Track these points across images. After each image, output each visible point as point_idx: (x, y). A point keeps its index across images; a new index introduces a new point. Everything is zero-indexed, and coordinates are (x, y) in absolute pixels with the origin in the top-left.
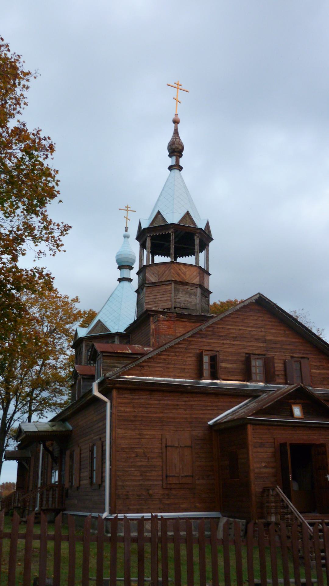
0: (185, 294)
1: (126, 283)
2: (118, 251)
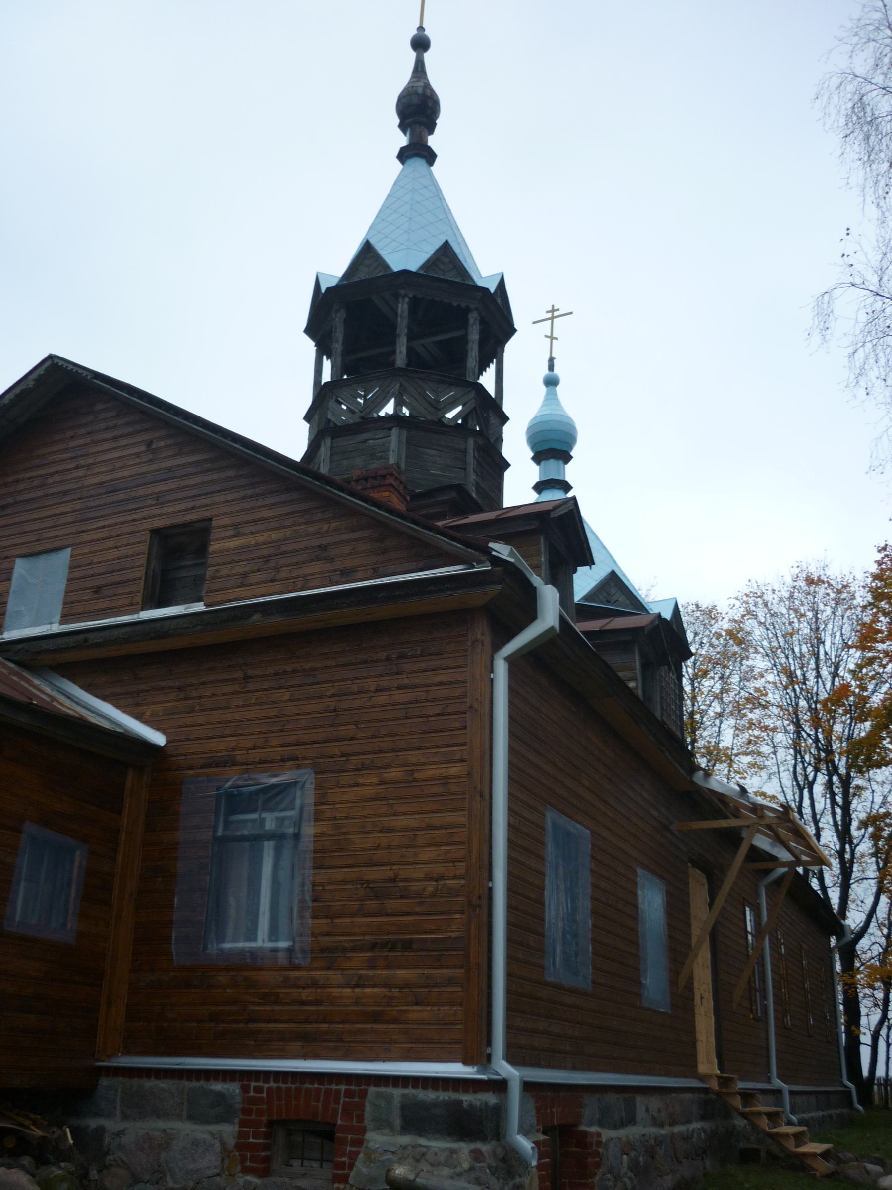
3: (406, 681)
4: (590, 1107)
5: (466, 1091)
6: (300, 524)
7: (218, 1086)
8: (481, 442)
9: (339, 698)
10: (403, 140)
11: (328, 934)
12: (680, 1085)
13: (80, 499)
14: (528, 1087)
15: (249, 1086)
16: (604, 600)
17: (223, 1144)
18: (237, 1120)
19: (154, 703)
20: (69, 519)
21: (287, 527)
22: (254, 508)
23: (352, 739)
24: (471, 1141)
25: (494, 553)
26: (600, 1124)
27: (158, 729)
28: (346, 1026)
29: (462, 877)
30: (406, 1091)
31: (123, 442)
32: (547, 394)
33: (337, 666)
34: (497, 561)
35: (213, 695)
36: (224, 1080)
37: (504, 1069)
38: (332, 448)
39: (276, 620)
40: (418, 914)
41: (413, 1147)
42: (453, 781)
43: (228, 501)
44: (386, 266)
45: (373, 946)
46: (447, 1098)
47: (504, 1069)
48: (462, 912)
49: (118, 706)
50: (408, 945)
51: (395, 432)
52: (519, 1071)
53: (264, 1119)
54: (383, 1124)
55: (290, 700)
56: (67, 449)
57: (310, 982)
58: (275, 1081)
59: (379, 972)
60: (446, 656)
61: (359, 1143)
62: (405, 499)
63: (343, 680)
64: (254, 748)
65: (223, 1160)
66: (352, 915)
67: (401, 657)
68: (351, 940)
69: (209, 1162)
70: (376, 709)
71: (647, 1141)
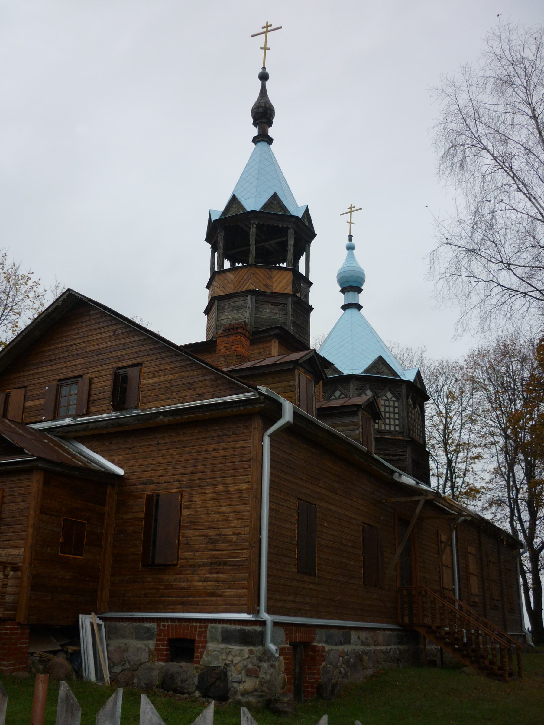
0: (232, 310)
1: (354, 311)
2: (340, 268)
3: (226, 446)
4: (320, 635)
5: (247, 625)
6: (181, 372)
7: (147, 625)
9: (197, 454)
10: (255, 131)
11: (193, 559)
12: (379, 627)
13: (84, 358)
14: (276, 624)
15: (160, 624)
16: (376, 372)
17: (149, 649)
18: (155, 639)
19: (119, 455)
20: (80, 367)
21: (175, 373)
22: (161, 364)
23: (203, 472)
24: (249, 646)
25: (259, 390)
26: (326, 642)
27: (121, 467)
28: (200, 598)
29: (247, 534)
30: (223, 625)
31: (103, 330)
32: (348, 255)
33: (197, 439)
34: (261, 394)
35: (144, 452)
36: (150, 622)
37: (265, 616)
38: (218, 306)
39: (168, 419)
40: (229, 550)
41: (226, 649)
42: (245, 491)
43: (150, 361)
44: (244, 209)
45: (211, 564)
46: (239, 628)
47: (265, 616)
48: (247, 549)
49: (104, 456)
50: (225, 563)
51: (249, 297)
52: (270, 617)
53: (166, 638)
54: (214, 639)
55: (177, 454)
56: (78, 333)
57: (185, 580)
58: (171, 622)
59: (213, 575)
60: (242, 435)
61: (204, 647)
62: (249, 338)
63: (200, 445)
64: (162, 476)
65: (149, 656)
66: (202, 551)
67: (224, 435)
68: (202, 562)
69: (144, 656)
70: (213, 459)
71: (357, 652)
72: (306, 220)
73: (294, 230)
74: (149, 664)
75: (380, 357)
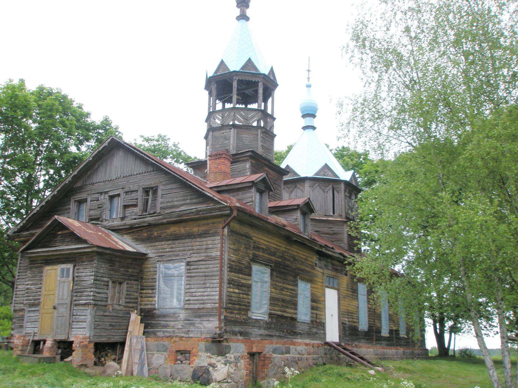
1: (310, 131)
8: (263, 130)
10: (238, 14)
72: (271, 76)
73: (263, 83)
74: (165, 365)
75: (326, 164)
